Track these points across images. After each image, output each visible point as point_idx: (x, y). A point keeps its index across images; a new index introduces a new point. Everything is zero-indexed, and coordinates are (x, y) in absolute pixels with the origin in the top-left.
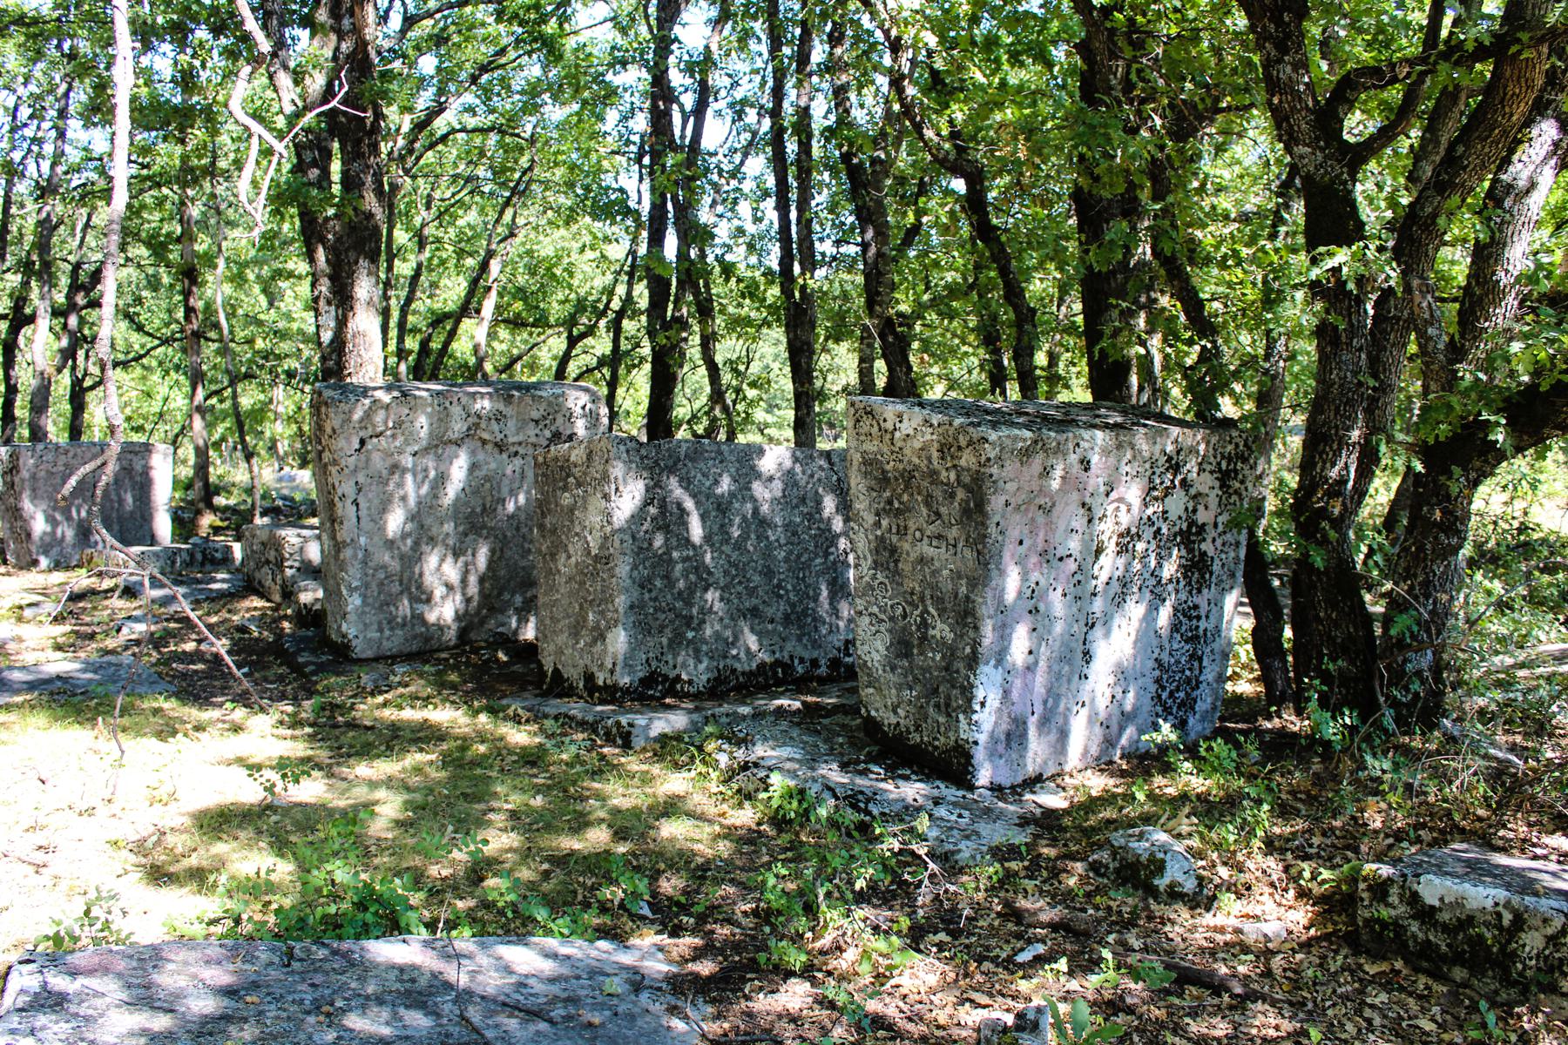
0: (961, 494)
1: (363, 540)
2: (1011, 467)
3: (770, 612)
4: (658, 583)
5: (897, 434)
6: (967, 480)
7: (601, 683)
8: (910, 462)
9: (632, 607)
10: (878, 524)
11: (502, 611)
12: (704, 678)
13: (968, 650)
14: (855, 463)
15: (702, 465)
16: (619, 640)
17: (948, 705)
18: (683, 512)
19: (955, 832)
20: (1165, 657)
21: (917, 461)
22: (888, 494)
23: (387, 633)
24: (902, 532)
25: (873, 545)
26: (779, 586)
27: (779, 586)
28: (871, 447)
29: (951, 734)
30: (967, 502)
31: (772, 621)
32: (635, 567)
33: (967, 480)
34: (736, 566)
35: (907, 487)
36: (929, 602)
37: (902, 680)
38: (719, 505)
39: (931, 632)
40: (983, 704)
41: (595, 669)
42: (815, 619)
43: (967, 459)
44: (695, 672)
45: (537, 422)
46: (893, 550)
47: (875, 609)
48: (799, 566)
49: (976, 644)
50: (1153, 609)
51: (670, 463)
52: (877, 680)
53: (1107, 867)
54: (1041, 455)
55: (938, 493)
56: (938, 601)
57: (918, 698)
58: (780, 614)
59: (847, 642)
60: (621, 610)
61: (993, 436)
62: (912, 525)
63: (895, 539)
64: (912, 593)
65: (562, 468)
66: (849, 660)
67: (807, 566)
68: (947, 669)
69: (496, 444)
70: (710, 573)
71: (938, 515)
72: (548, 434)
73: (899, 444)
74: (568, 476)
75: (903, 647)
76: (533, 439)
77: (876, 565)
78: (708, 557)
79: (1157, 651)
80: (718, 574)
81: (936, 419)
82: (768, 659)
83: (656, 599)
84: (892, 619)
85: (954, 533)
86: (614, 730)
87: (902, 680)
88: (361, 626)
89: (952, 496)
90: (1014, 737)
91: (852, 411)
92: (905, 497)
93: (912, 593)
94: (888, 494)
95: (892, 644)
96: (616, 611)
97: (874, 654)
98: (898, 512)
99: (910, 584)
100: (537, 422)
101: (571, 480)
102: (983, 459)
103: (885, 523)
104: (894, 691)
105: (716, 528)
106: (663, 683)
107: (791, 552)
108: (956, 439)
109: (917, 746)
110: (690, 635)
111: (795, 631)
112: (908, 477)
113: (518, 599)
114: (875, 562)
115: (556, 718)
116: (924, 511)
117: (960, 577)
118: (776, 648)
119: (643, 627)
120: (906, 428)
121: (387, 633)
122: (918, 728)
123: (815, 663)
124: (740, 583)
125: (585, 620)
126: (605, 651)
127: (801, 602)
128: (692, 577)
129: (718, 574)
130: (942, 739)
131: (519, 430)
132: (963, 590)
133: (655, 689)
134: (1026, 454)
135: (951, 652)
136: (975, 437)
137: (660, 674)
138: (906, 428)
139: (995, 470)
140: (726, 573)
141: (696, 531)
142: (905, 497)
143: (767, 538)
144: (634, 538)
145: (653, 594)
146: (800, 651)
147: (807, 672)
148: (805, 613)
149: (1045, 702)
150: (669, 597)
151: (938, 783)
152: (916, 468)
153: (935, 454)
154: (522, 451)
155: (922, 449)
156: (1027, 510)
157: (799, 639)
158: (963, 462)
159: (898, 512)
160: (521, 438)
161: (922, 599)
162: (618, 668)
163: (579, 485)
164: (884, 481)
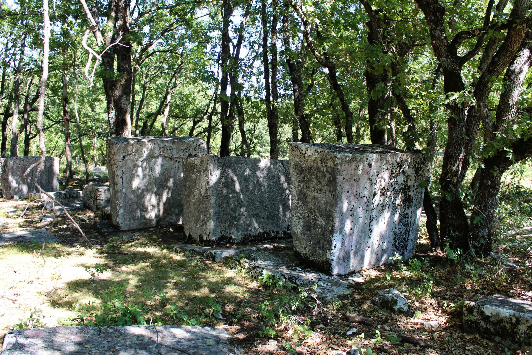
0: (328, 175)
1: (124, 190)
2: (345, 166)
3: (262, 215)
4: (225, 205)
5: (306, 155)
6: (330, 170)
8: (310, 164)
9: (215, 213)
10: (299, 186)
11: (171, 215)
12: (240, 237)
13: (330, 228)
17: (323, 247)
20: (397, 231)
22: (303, 175)
23: (132, 222)
24: (308, 188)
26: (266, 206)
27: (266, 206)
28: (297, 159)
30: (330, 178)
32: (217, 200)
33: (330, 170)
34: (251, 200)
35: (310, 173)
36: (317, 212)
38: (245, 179)
40: (335, 247)
41: (203, 234)
42: (278, 218)
43: (330, 163)
44: (236, 235)
45: (183, 150)
46: (305, 194)
47: (298, 214)
48: (272, 200)
49: (333, 226)
50: (393, 214)
51: (229, 164)
52: (299, 238)
54: (355, 162)
55: (320, 175)
56: (320, 212)
57: (313, 245)
58: (266, 216)
60: (212, 214)
62: (311, 186)
63: (305, 190)
65: (192, 166)
67: (275, 200)
68: (323, 235)
69: (169, 158)
70: (242, 202)
71: (320, 182)
72: (187, 154)
73: (307, 159)
74: (194, 169)
75: (308, 227)
76: (182, 156)
77: (299, 199)
79: (394, 229)
80: (245, 202)
83: (224, 211)
84: (304, 218)
85: (325, 188)
88: (123, 219)
89: (325, 176)
90: (345, 258)
92: (309, 176)
93: (311, 209)
94: (303, 175)
96: (210, 215)
99: (310, 206)
100: (183, 150)
101: (195, 170)
102: (335, 163)
103: (302, 185)
105: (244, 187)
106: (226, 239)
107: (270, 195)
109: (313, 261)
110: (235, 223)
111: (271, 222)
112: (310, 169)
113: (177, 211)
114: (298, 198)
115: (190, 251)
116: (315, 181)
117: (327, 204)
118: (265, 227)
119: (219, 220)
120: (309, 153)
121: (132, 222)
122: (313, 255)
123: (278, 233)
125: (200, 217)
126: (206, 228)
129: (245, 202)
131: (177, 153)
133: (223, 241)
135: (324, 229)
136: (333, 156)
137: (225, 236)
138: (309, 153)
139: (339, 167)
141: (238, 187)
142: (309, 176)
144: (216, 190)
145: (223, 209)
146: (272, 228)
148: (274, 215)
153: (319, 162)
154: (178, 160)
155: (314, 160)
157: (272, 224)
158: (328, 165)
160: (178, 156)
161: (314, 211)
162: (211, 234)
163: (198, 172)
164: (302, 171)
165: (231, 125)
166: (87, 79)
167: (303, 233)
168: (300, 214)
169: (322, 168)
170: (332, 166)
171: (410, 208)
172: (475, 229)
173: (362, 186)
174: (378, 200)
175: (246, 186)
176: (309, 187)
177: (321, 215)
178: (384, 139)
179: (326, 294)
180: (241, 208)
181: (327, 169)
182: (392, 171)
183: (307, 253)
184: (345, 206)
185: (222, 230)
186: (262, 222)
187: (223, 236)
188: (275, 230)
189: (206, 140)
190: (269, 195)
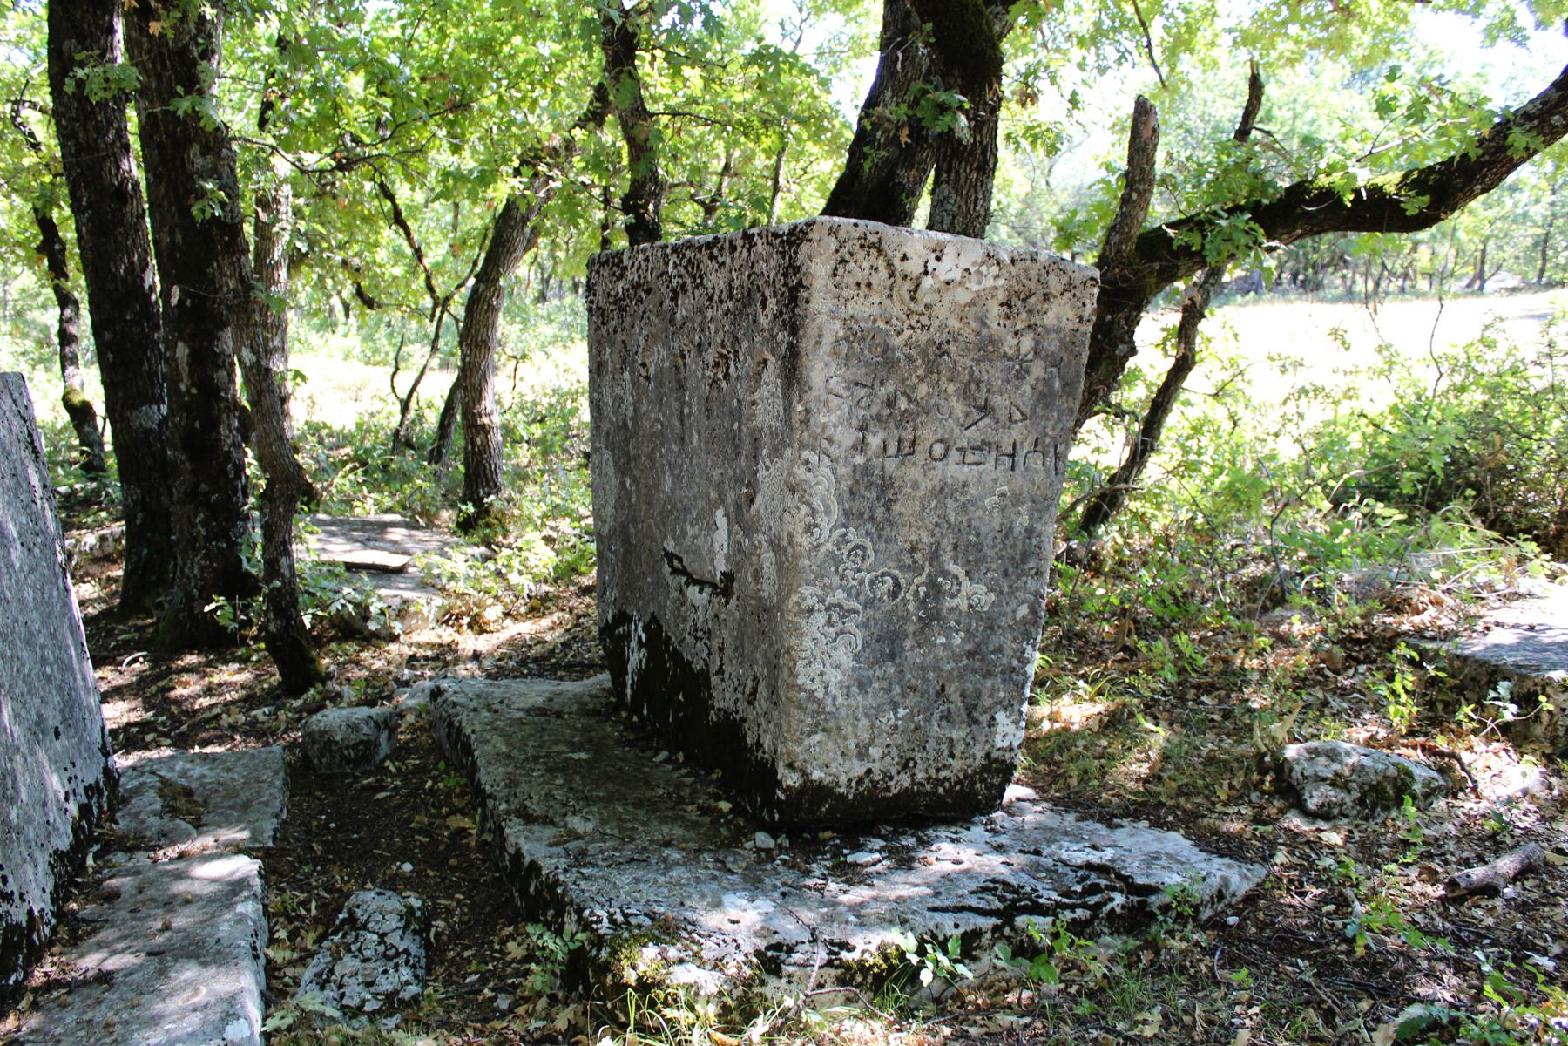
0: (1038, 370)
5: (927, 282)
8: (943, 327)
10: (861, 446)
13: (1023, 611)
14: (828, 339)
21: (954, 324)
28: (863, 308)
30: (1047, 382)
35: (932, 369)
47: (840, 595)
55: (993, 374)
57: (911, 716)
62: (928, 434)
63: (891, 465)
64: (913, 550)
71: (986, 409)
73: (927, 300)
89: (1022, 374)
94: (890, 388)
95: (865, 645)
103: (875, 441)
109: (906, 794)
112: (935, 355)
116: (959, 407)
122: (905, 766)
142: (923, 389)
152: (954, 337)
153: (995, 310)
155: (971, 304)
158: (1050, 319)
161: (934, 555)
168: (848, 592)
181: (1037, 342)
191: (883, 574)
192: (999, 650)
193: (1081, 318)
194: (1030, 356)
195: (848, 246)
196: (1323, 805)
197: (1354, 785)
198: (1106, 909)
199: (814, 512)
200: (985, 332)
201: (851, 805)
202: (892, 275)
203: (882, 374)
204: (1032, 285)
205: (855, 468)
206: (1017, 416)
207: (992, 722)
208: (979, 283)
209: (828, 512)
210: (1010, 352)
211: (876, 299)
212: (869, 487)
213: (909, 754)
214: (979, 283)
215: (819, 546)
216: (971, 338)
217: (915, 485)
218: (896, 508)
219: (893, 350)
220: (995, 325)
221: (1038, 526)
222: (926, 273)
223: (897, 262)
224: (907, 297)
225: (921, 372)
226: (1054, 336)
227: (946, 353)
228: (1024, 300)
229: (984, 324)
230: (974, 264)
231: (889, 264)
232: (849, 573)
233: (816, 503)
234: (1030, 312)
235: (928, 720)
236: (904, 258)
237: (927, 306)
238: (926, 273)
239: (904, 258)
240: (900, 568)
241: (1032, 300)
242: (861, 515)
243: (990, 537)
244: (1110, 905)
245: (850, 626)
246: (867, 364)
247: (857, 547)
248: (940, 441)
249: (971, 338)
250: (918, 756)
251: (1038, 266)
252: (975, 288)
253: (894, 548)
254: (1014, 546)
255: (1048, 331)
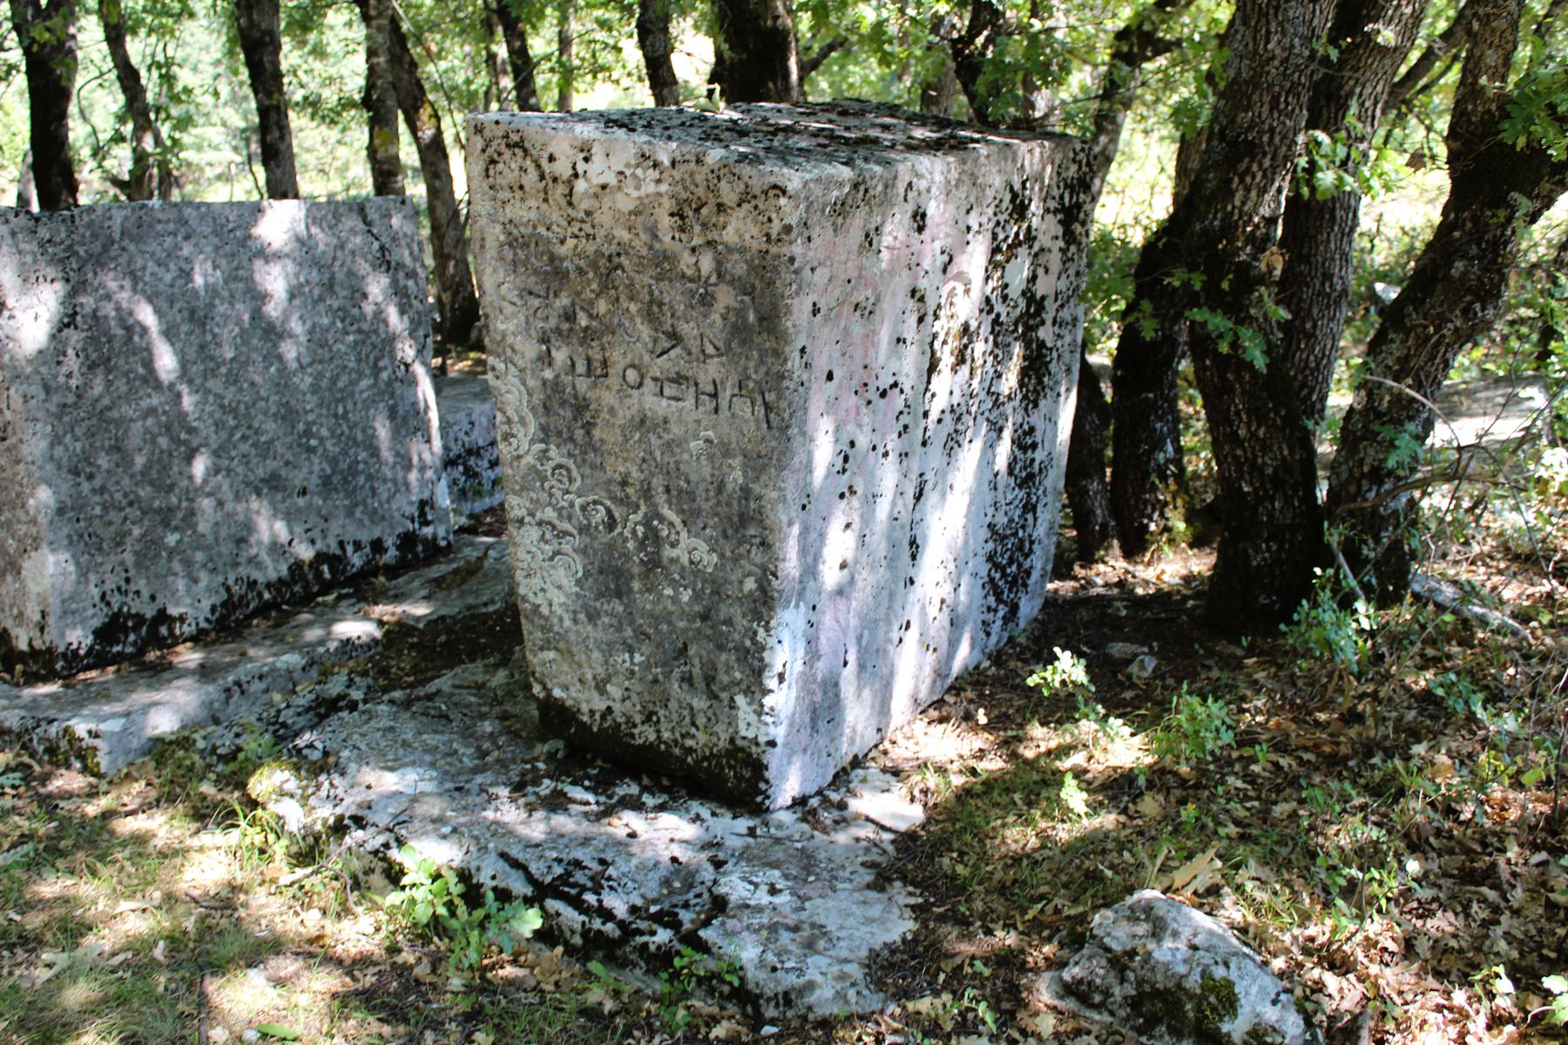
0: (725, 297)
2: (822, 234)
3: (297, 478)
4: (103, 461)
5: (580, 186)
6: (740, 269)
7: (23, 646)
8: (609, 238)
9: (61, 511)
10: (546, 359)
12: (206, 605)
13: (750, 585)
14: (490, 243)
15: (153, 246)
16: (50, 569)
17: (710, 680)
18: (132, 328)
19: (785, 937)
20: (1001, 520)
21: (624, 235)
22: (564, 301)
24: (599, 371)
25: (538, 398)
26: (308, 434)
27: (308, 434)
28: (523, 212)
29: (719, 728)
30: (740, 312)
31: (304, 492)
32: (56, 440)
33: (740, 269)
34: (234, 411)
35: (606, 284)
36: (661, 499)
37: (611, 636)
38: (192, 312)
39: (668, 552)
40: (781, 678)
42: (370, 478)
43: (739, 229)
44: (192, 602)
46: (581, 407)
47: (550, 514)
48: (334, 397)
49: (767, 574)
50: (990, 446)
51: (96, 247)
52: (562, 637)
53: (1107, 994)
54: (864, 210)
55: (674, 296)
56: (684, 499)
57: (647, 666)
58: (314, 479)
59: (423, 504)
60: (43, 520)
61: (794, 179)
62: (618, 358)
63: (583, 385)
64: (624, 483)
66: (428, 531)
67: (347, 394)
68: (705, 617)
70: (192, 431)
71: (675, 337)
73: (584, 205)
75: (609, 578)
77: (546, 434)
78: (188, 402)
79: (991, 511)
80: (206, 429)
81: (664, 152)
82: (305, 553)
83: (103, 490)
84: (584, 530)
85: (711, 371)
86: (64, 745)
87: (611, 636)
89: (707, 301)
90: (823, 709)
91: (479, 143)
92: (602, 306)
93: (624, 483)
94: (564, 301)
95: (587, 574)
96: (34, 521)
97: (553, 593)
98: (588, 336)
99: (615, 468)
102: (776, 227)
103: (560, 356)
104: (596, 655)
105: (192, 353)
106: (136, 629)
107: (320, 375)
108: (712, 190)
109: (649, 748)
110: (172, 539)
111: (341, 501)
112: (607, 268)
114: (544, 428)
116: (645, 331)
117: (727, 453)
118: (316, 534)
119: (86, 533)
120: (599, 171)
122: (649, 718)
123: (378, 546)
124: (244, 438)
126: (23, 591)
127: (345, 453)
128: (163, 442)
129: (206, 429)
130: (702, 737)
132: (736, 477)
133: (132, 644)
134: (841, 209)
135: (713, 589)
136: (757, 185)
137: (129, 616)
138: (599, 171)
139: (797, 249)
140: (219, 425)
141: (166, 361)
142: (602, 306)
143: (280, 358)
144: (47, 389)
145: (97, 483)
146: (353, 532)
147: (369, 562)
148: (353, 470)
149: (859, 639)
150: (126, 481)
151: (696, 807)
152: (624, 249)
153: (666, 222)
155: (636, 213)
156: (839, 315)
157: (350, 513)
158: (729, 235)
159: (588, 336)
161: (647, 493)
162: (51, 620)
164: (555, 275)
165: (61, 44)
166: (1544, 658)
167: (585, 607)
168: (560, 510)
169: (687, 260)
170: (757, 244)
171: (1042, 403)
172: (1365, 484)
173: (885, 336)
174: (946, 386)
175: (202, 347)
176: (605, 363)
177: (690, 518)
178: (786, 74)
179: (800, 972)
180: (189, 458)
181: (719, 263)
182: (995, 236)
183: (617, 707)
184: (823, 452)
185: (109, 586)
186: (299, 510)
187: (115, 617)
188: (365, 537)
189: (633, 55)
190: (319, 376)
191: (595, 502)
192: (729, 622)
193: (768, 235)
194: (713, 279)
195: (494, 144)
196: (1081, 981)
197: (1131, 976)
198: (640, 940)
199: (509, 421)
200: (657, 246)
201: (596, 736)
202: (542, 177)
203: (555, 285)
204: (701, 192)
205: (544, 382)
206: (710, 350)
207: (732, 705)
208: (638, 188)
209: (523, 422)
210: (689, 273)
211: (533, 203)
212: (563, 403)
213: (651, 707)
214: (638, 188)
215: (519, 457)
216: (644, 252)
217: (612, 411)
218: (597, 433)
219: (562, 260)
220: (667, 239)
221: (756, 488)
222: (576, 176)
223: (544, 163)
224: (563, 202)
225: (594, 286)
226: (737, 256)
227: (619, 266)
228: (697, 210)
229: (655, 237)
230: (628, 165)
231: (539, 166)
232: (559, 494)
233: (510, 412)
234: (704, 225)
235: (667, 675)
236: (551, 159)
237: (588, 213)
238: (576, 176)
239: (551, 159)
240: (613, 499)
241: (704, 211)
242: (559, 434)
243: (702, 486)
244: (645, 938)
245: (566, 548)
246: (536, 272)
247: (559, 466)
248: (633, 366)
249: (644, 252)
250: (661, 712)
251: (705, 170)
252: (635, 194)
253: (602, 477)
254: (729, 504)
255: (729, 250)
